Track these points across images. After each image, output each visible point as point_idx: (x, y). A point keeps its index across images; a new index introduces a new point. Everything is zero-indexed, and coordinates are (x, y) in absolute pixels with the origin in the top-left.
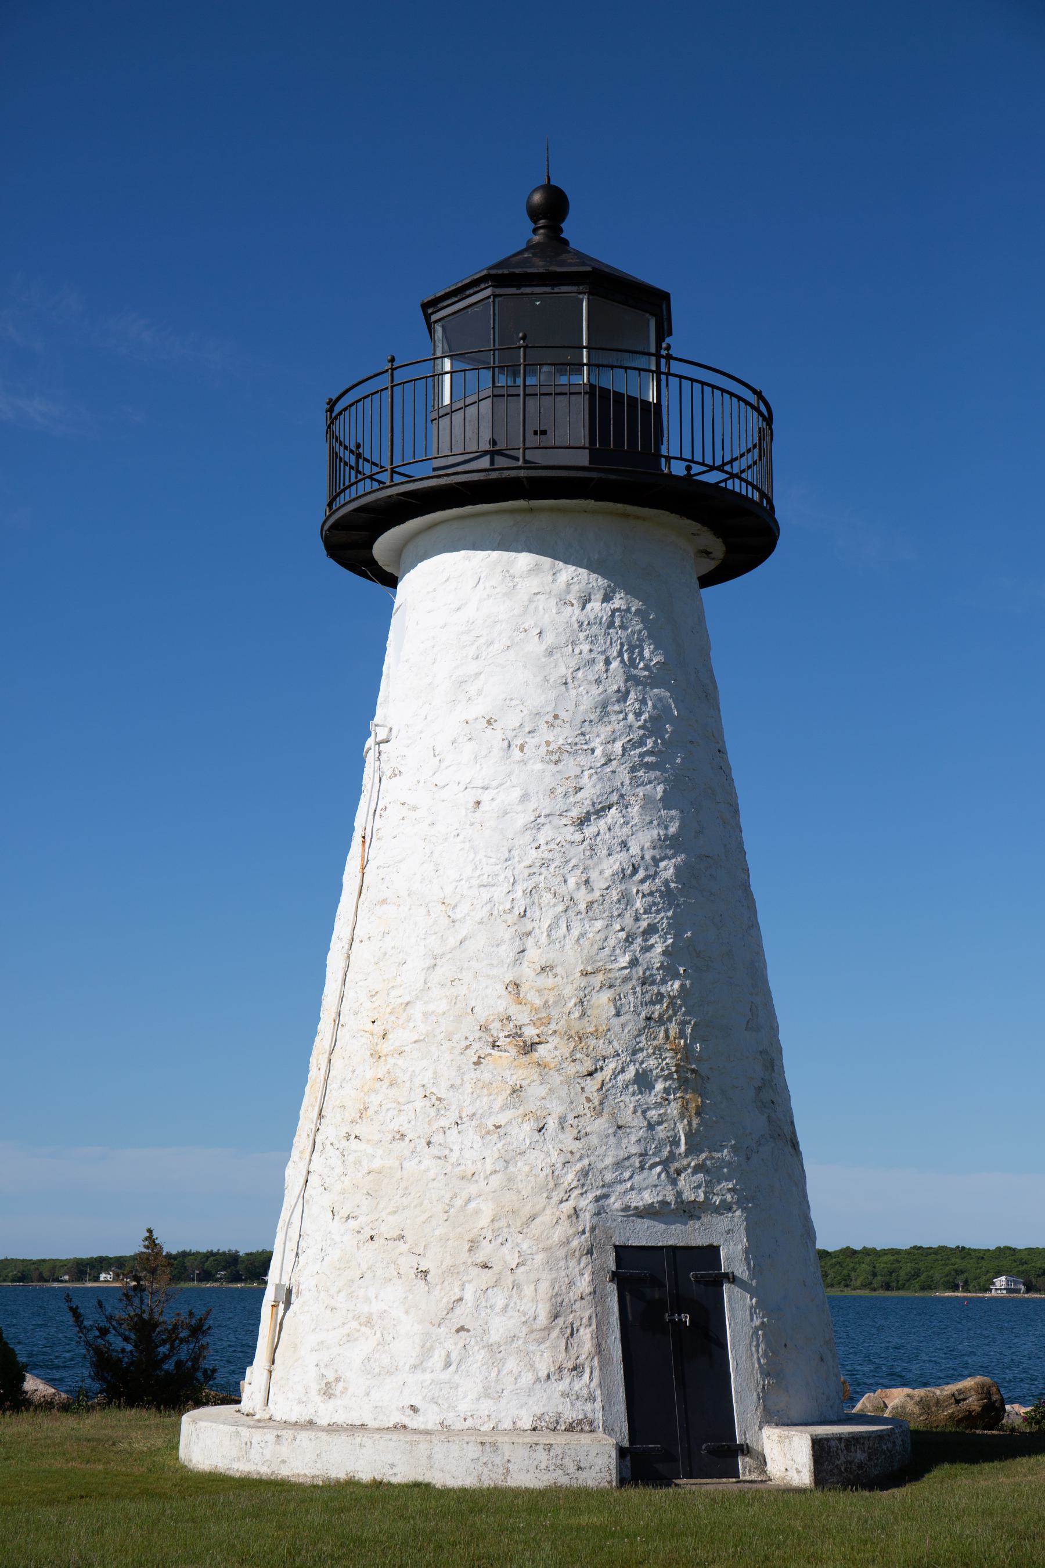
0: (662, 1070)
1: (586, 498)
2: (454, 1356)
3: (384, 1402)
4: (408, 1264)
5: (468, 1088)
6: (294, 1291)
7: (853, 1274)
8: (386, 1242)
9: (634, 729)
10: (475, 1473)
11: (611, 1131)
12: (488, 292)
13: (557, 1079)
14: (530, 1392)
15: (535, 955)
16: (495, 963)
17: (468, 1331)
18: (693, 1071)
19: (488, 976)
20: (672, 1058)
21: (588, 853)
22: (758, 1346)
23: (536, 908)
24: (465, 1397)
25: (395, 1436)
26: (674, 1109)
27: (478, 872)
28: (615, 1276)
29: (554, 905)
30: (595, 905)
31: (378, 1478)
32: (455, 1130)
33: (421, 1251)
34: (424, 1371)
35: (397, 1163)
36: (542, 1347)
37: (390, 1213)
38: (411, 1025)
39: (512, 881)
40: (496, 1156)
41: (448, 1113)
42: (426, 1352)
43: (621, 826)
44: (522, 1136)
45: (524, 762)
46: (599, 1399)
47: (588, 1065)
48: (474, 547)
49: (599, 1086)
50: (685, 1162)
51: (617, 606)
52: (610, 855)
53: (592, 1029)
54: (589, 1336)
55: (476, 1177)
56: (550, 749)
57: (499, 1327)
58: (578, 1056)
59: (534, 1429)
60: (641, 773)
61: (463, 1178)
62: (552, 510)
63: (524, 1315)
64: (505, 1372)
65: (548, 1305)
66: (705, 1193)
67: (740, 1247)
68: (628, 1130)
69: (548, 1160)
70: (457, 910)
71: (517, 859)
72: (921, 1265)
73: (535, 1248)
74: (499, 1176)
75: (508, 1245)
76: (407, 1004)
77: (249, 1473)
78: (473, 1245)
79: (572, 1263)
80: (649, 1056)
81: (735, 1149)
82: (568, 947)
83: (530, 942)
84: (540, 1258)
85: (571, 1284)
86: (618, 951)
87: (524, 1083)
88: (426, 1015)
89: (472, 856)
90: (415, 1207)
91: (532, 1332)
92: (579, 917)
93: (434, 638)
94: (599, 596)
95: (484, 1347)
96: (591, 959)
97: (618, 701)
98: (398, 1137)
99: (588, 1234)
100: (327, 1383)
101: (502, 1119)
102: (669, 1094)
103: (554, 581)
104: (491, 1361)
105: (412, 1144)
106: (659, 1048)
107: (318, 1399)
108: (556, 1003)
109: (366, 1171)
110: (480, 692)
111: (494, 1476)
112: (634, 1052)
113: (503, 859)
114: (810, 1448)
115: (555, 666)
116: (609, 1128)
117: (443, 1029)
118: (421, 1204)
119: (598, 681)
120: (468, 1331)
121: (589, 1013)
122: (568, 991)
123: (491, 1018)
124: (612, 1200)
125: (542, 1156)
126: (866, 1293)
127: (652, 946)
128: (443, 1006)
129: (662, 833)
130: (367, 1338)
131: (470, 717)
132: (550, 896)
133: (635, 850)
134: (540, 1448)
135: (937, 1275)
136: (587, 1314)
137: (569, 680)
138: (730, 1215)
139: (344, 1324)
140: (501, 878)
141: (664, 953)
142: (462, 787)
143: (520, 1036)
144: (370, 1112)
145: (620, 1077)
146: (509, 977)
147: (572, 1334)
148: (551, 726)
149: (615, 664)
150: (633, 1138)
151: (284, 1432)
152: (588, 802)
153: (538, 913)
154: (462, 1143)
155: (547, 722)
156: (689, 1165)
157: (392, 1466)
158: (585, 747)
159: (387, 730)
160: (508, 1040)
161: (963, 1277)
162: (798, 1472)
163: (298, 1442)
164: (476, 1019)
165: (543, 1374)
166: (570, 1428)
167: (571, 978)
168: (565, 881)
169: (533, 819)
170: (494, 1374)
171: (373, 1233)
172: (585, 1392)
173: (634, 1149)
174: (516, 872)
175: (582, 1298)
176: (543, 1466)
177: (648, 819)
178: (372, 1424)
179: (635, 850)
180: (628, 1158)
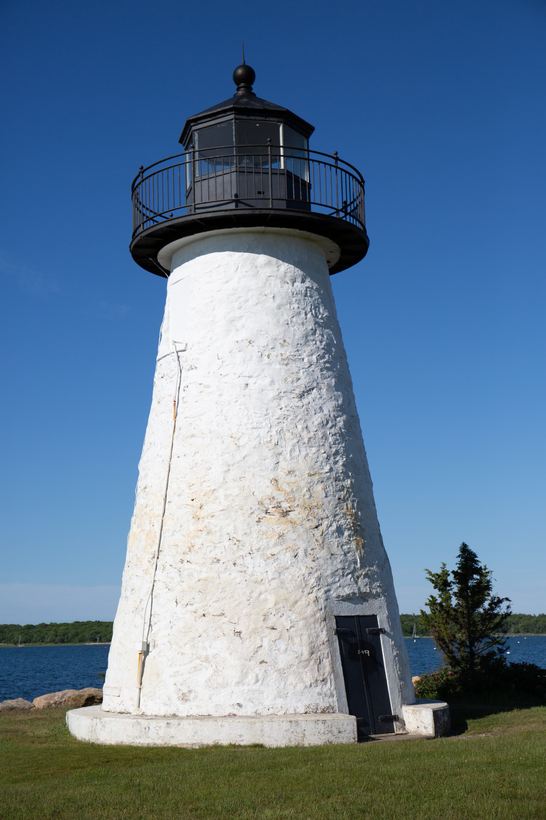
0: (347, 525)
1: (295, 228)
2: (260, 677)
3: (223, 702)
4: (229, 629)
5: (255, 535)
6: (151, 645)
7: (46, 636)
8: (214, 617)
9: (320, 349)
10: (287, 738)
11: (329, 557)
12: (232, 116)
13: (301, 530)
14: (302, 693)
15: (283, 464)
16: (264, 469)
17: (266, 663)
18: (359, 526)
19: (261, 476)
20: (351, 519)
21: (306, 412)
22: (396, 665)
23: (283, 440)
24: (268, 698)
25: (230, 720)
26: (353, 545)
27: (251, 421)
28: (338, 633)
29: (292, 439)
30: (312, 439)
31: (233, 743)
32: (249, 557)
33: (236, 621)
34: (243, 685)
35: (217, 575)
36: (306, 670)
37: (214, 602)
38: (218, 501)
39: (269, 426)
40: (274, 570)
41: (244, 548)
42: (244, 675)
43: (319, 399)
44: (286, 559)
45: (270, 364)
46: (335, 696)
47: (315, 523)
48: (234, 250)
49: (321, 533)
50: (360, 573)
51: (307, 285)
52: (315, 414)
53: (315, 504)
54: (328, 663)
55: (263, 582)
56: (283, 357)
57: (283, 660)
58: (310, 518)
59: (306, 713)
60: (325, 372)
61: (256, 582)
62: (263, 232)
63: (296, 653)
64: (288, 684)
65: (308, 648)
66: (370, 588)
67: (385, 615)
68: (336, 556)
69: (301, 572)
70: (241, 441)
71: (271, 415)
72: (79, 631)
73: (298, 618)
74: (276, 581)
75: (284, 617)
76: (214, 490)
77: (148, 744)
78: (266, 617)
79: (317, 625)
80: (341, 518)
81: (378, 566)
82: (300, 461)
83: (281, 458)
84: (301, 623)
85: (318, 636)
86: (324, 464)
87: (285, 532)
88: (226, 496)
89: (246, 412)
90: (230, 598)
91: (301, 662)
92: (304, 445)
93: (212, 297)
94: (300, 280)
95: (276, 671)
96: (312, 468)
97: (312, 334)
98: (215, 561)
99: (323, 610)
100: (183, 694)
101: (275, 551)
102: (350, 538)
103: (278, 270)
104: (280, 678)
105: (225, 565)
106: (345, 514)
107: (179, 703)
108: (297, 490)
109: (197, 579)
110: (243, 326)
111: (297, 738)
112: (335, 516)
113: (264, 414)
114: (432, 716)
115: (282, 315)
116: (328, 555)
117: (237, 503)
118: (233, 597)
119: (303, 324)
120: (266, 663)
121: (313, 495)
122: (302, 484)
123: (264, 498)
124: (332, 592)
125: (298, 570)
126: (52, 645)
127: (338, 461)
128: (236, 491)
129: (336, 403)
130: (207, 669)
131: (239, 339)
132: (290, 434)
133: (326, 412)
134: (320, 722)
135: (87, 635)
136: (326, 651)
137: (289, 322)
138: (380, 599)
139: (191, 661)
140: (264, 424)
141: (343, 465)
142: (237, 376)
143: (280, 507)
144: (196, 548)
145: (330, 529)
146: (272, 476)
147: (320, 663)
148: (282, 346)
149: (309, 315)
150: (339, 561)
151: (171, 721)
152: (303, 386)
153: (284, 443)
154: (254, 564)
155: (280, 344)
156: (362, 574)
157: (241, 736)
158: (300, 357)
159: (184, 345)
160: (274, 509)
161: (99, 635)
162: (425, 728)
163: (181, 726)
164: (256, 498)
165: (308, 684)
166: (323, 712)
167: (303, 477)
168: (296, 427)
169: (277, 394)
170: (282, 685)
171: (204, 613)
172: (329, 692)
173: (340, 566)
174: (271, 421)
175: (323, 644)
176: (322, 732)
177: (330, 396)
178: (214, 714)
179: (326, 412)
180: (337, 570)
